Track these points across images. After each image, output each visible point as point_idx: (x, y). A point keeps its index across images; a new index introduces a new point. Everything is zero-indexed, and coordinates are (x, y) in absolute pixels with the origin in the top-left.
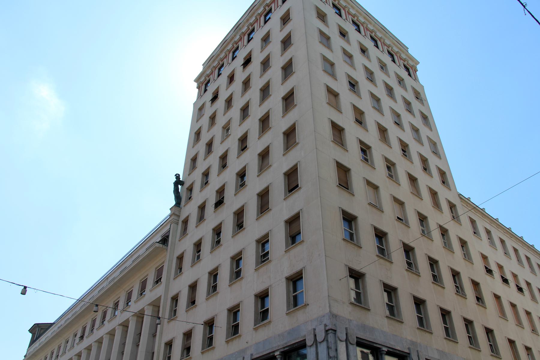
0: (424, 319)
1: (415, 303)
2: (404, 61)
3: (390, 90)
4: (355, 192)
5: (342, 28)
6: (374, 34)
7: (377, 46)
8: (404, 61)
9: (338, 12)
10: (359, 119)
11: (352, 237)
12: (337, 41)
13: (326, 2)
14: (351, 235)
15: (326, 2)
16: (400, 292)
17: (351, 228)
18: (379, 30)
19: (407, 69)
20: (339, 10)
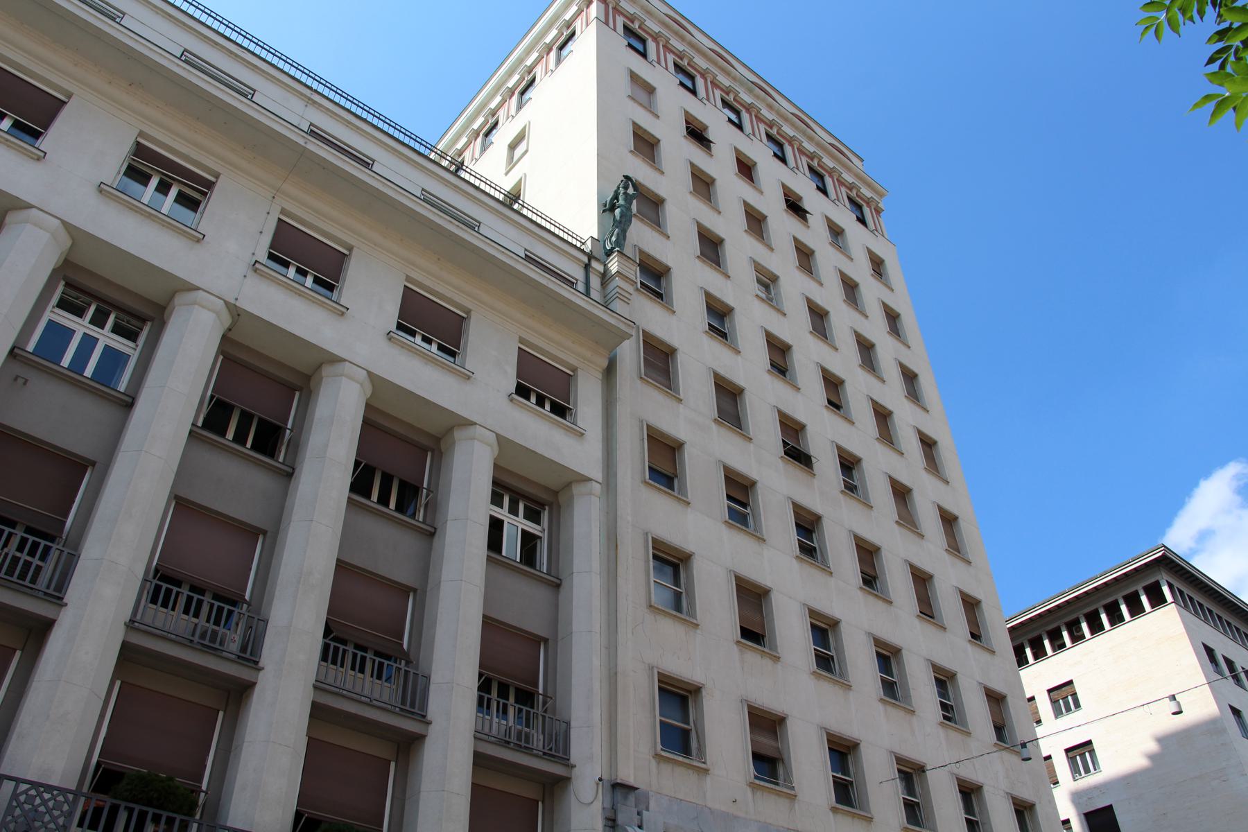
0: (693, 735)
1: (961, 791)
2: (851, 190)
3: (850, 288)
4: (893, 596)
5: (790, 190)
6: (854, 192)
7: (824, 191)
8: (851, 190)
9: (733, 117)
10: (834, 400)
11: (680, 604)
12: (730, 185)
13: (708, 99)
14: (678, 596)
15: (708, 99)
16: (988, 793)
17: (677, 582)
18: (786, 120)
19: (856, 205)
20: (780, 146)
